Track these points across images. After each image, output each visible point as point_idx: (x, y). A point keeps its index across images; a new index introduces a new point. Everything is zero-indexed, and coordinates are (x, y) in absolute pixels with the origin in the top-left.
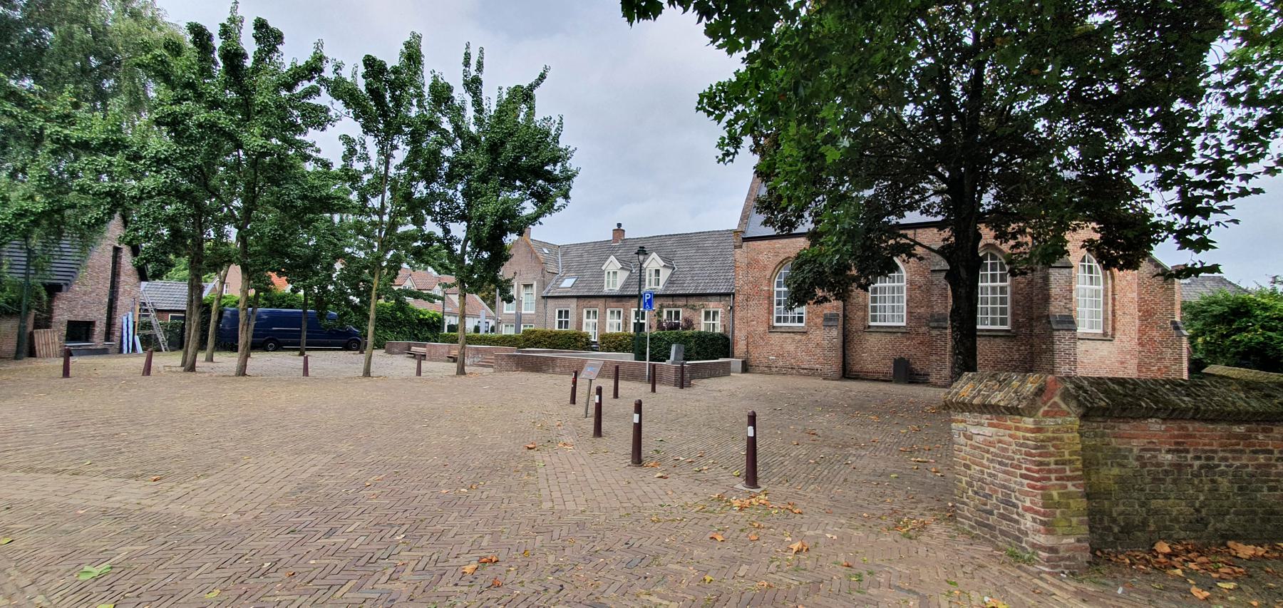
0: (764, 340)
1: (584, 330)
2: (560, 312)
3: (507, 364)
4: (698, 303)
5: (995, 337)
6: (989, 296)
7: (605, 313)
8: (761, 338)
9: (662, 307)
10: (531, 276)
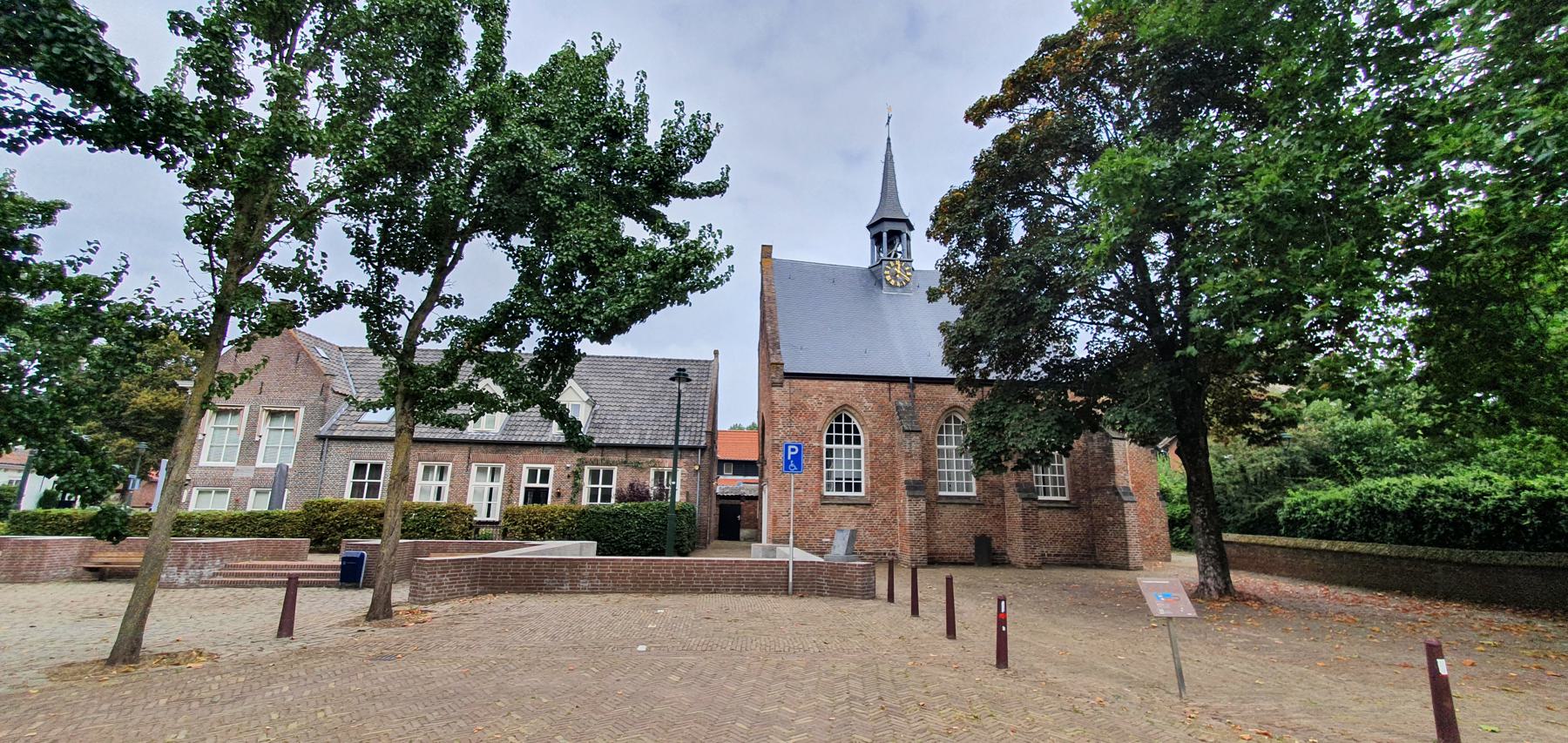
0: (814, 515)
1: (470, 501)
2: (360, 468)
3: (453, 579)
4: (645, 459)
5: (1062, 508)
6: (843, 459)
7: (468, 469)
8: (812, 513)
9: (582, 463)
10: (295, 396)
